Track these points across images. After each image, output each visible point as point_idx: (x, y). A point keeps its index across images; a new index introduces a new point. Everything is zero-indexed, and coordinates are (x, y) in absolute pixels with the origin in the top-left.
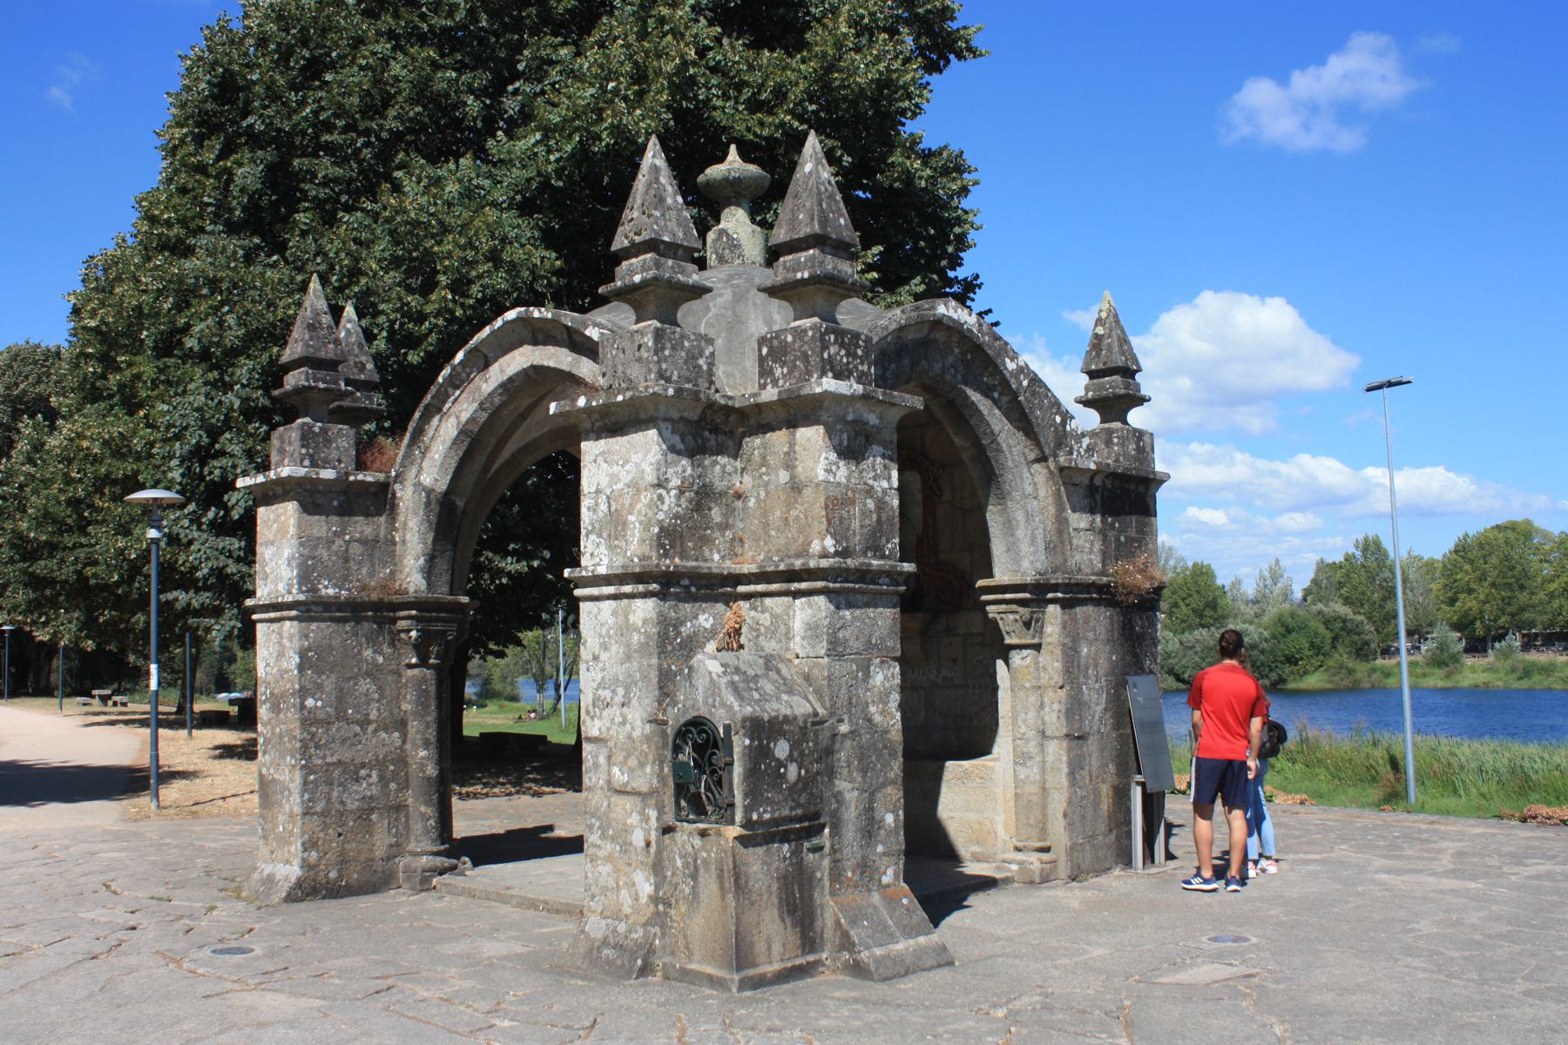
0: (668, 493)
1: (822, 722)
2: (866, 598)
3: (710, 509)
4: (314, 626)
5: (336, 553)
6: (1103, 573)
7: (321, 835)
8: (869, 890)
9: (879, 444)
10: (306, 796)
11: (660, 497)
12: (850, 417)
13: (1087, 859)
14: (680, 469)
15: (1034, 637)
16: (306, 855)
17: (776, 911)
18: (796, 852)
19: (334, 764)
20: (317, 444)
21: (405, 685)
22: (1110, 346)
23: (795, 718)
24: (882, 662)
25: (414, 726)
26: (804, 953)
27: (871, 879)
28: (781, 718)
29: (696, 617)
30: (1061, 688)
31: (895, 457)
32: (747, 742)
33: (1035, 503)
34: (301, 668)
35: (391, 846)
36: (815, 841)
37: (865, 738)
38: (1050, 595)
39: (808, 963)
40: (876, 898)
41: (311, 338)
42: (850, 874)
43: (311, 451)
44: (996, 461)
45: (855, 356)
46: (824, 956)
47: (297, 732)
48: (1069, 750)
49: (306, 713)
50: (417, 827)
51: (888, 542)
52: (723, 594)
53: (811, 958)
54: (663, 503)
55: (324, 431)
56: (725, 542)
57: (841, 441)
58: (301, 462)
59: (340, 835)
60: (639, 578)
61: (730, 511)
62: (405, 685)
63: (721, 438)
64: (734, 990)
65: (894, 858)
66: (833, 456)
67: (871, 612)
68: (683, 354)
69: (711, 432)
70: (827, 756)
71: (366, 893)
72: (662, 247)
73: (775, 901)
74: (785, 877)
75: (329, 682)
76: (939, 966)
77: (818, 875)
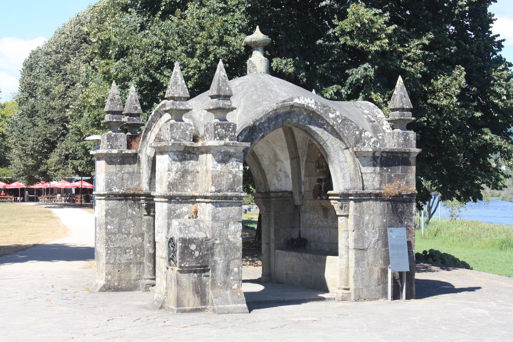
0: (172, 172)
1: (209, 240)
2: (228, 204)
3: (187, 177)
4: (111, 202)
5: (119, 177)
6: (380, 189)
7: (112, 271)
8: (227, 290)
9: (235, 157)
10: (107, 258)
11: (169, 174)
12: (222, 151)
13: (365, 293)
14: (176, 165)
15: (344, 212)
16: (107, 277)
17: (191, 292)
18: (200, 276)
19: (117, 247)
20: (113, 141)
21: (144, 222)
22: (397, 98)
23: (199, 238)
24: (234, 223)
25: (146, 236)
26: (201, 305)
27: (228, 287)
28: (193, 238)
29: (182, 208)
30: (353, 231)
31: (242, 161)
32: (181, 244)
33: (345, 164)
34: (106, 216)
35: (137, 276)
36: (207, 274)
37: (226, 245)
38: (350, 198)
39: (202, 308)
40: (228, 292)
41: (111, 104)
42: (219, 284)
43: (111, 143)
44: (327, 150)
45: (229, 131)
46: (208, 307)
47: (105, 237)
48: (356, 254)
49: (107, 230)
50: (146, 270)
51: (237, 187)
52: (191, 201)
53: (203, 307)
54: (170, 176)
55: (115, 136)
56: (193, 186)
57: (219, 158)
58: (107, 147)
59: (119, 271)
60: (164, 197)
61: (194, 176)
62: (144, 222)
63: (191, 155)
64: (175, 312)
65: (238, 281)
66: (216, 163)
67: (230, 208)
68: (181, 130)
69: (188, 154)
70: (211, 250)
71: (128, 291)
72: (175, 98)
73: (191, 289)
74: (195, 283)
75: (116, 221)
76: (242, 313)
77: (208, 283)
